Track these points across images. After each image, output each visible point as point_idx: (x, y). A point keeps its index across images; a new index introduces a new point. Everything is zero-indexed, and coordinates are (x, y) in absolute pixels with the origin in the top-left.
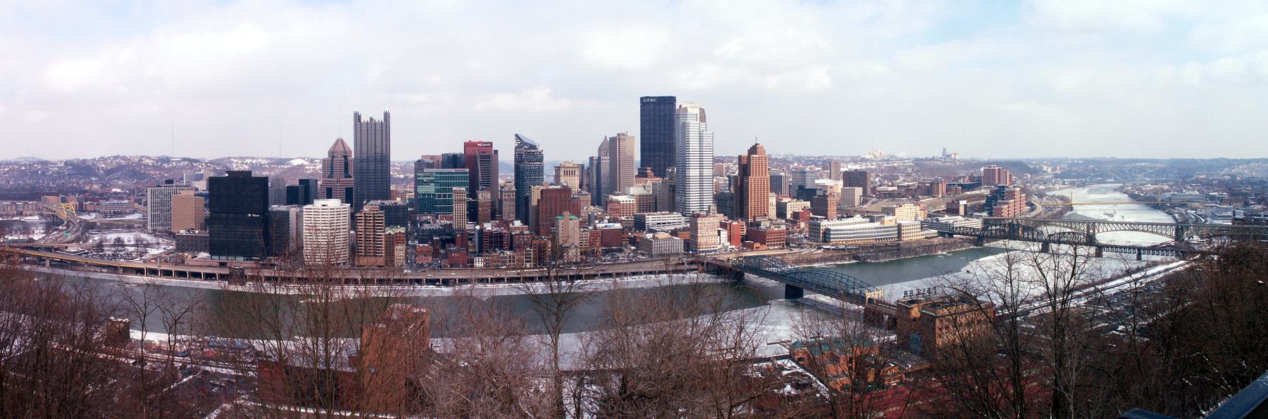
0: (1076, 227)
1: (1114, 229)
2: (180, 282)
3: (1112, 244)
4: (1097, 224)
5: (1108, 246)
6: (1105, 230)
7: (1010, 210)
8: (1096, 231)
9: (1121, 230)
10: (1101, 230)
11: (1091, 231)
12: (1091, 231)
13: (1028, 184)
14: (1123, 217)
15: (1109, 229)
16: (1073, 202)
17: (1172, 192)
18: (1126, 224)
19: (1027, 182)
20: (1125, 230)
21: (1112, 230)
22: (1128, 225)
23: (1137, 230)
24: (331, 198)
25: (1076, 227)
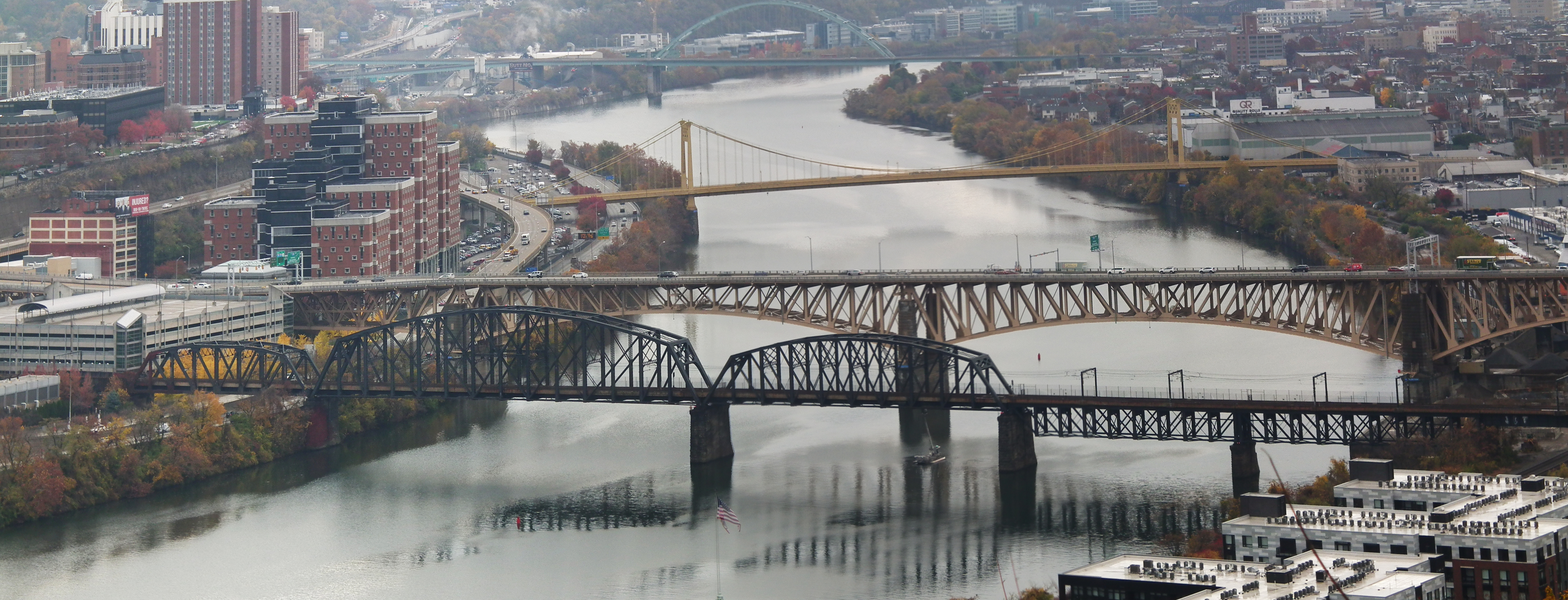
5: (1064, 404)
23: (1183, 313)
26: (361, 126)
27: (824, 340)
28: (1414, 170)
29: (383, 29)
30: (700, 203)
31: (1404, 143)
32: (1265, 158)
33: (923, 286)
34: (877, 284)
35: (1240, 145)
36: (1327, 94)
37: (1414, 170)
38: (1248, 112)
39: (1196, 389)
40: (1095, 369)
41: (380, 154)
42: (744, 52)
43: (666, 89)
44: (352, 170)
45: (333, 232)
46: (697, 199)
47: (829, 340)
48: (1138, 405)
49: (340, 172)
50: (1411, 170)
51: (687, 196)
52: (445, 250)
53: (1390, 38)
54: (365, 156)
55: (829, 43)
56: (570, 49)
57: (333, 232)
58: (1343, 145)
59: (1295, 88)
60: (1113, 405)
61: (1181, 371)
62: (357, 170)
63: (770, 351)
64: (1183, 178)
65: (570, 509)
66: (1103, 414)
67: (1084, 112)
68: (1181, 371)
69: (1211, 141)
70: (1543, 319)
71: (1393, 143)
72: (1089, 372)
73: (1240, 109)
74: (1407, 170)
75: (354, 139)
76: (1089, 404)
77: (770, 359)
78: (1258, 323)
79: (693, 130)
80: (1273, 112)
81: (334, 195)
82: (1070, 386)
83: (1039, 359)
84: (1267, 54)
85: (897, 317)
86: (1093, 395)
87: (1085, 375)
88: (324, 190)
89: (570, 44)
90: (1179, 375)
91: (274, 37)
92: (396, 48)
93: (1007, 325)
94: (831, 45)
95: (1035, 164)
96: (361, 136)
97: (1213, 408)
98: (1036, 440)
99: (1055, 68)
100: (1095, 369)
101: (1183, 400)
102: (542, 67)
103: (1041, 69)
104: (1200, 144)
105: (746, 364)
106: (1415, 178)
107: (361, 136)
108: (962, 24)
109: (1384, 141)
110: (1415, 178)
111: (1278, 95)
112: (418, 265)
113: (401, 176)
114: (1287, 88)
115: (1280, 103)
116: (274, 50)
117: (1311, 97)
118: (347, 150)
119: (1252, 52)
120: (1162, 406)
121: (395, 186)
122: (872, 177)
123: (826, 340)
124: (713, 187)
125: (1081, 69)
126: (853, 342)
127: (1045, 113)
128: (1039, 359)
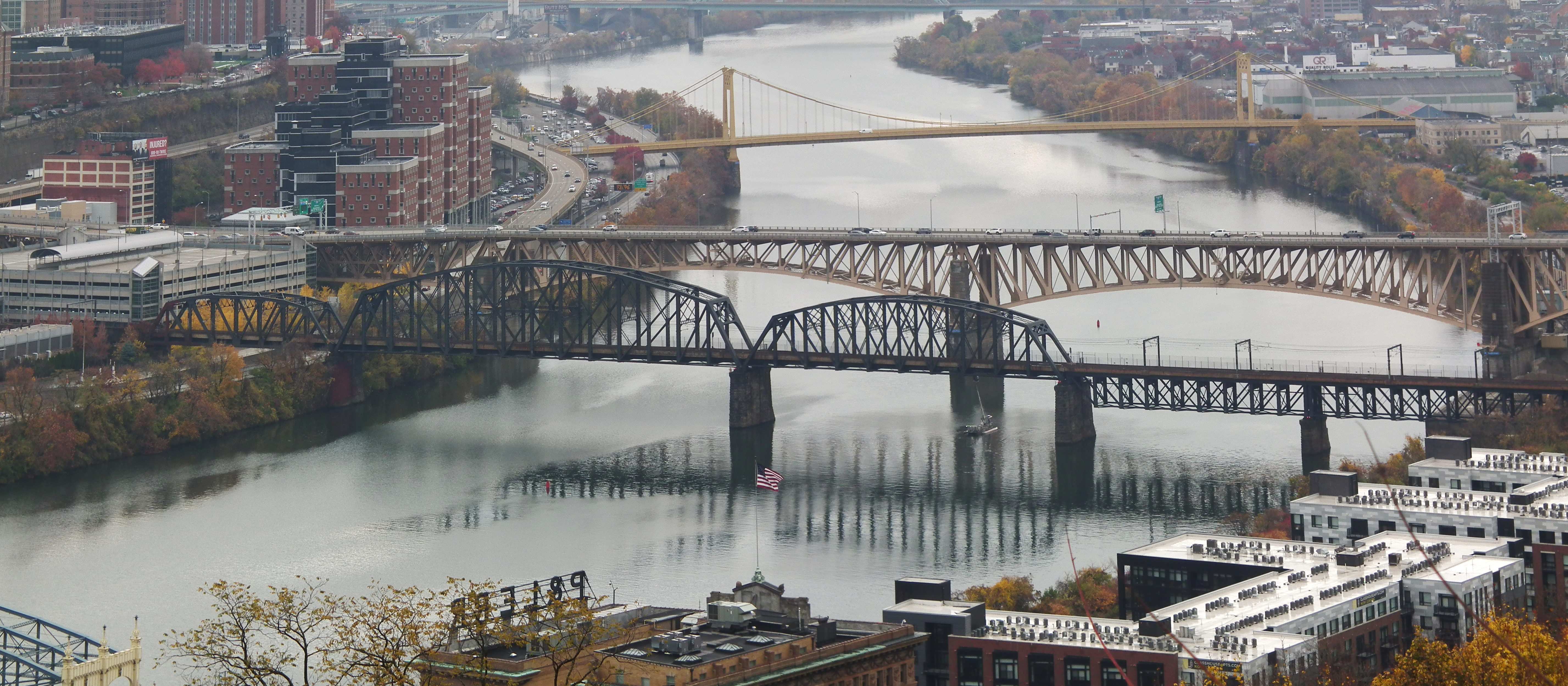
5: (1125, 374)
23: (1252, 279)
26: (389, 69)
27: (871, 301)
28: (1496, 133)
30: (742, 154)
31: (1485, 104)
32: (1339, 117)
35: (1314, 103)
36: (1405, 51)
37: (1496, 133)
38: (1322, 69)
41: (408, 98)
44: (379, 115)
48: (1203, 377)
49: (367, 116)
50: (1492, 132)
51: (729, 147)
52: (475, 200)
54: (393, 100)
60: (1177, 376)
61: (1249, 341)
63: (814, 312)
64: (1253, 137)
68: (1249, 341)
73: (1314, 65)
74: (1489, 133)
75: (381, 83)
77: (814, 320)
79: (736, 78)
80: (1348, 69)
82: (1132, 356)
83: (1098, 326)
84: (1342, 7)
86: (1156, 364)
87: (1147, 344)
88: (350, 136)
90: (1247, 345)
93: (1066, 289)
96: (389, 80)
97: (1282, 380)
99: (1119, 17)
101: (1251, 372)
102: (578, 10)
103: (1104, 18)
105: (789, 325)
107: (389, 80)
112: (447, 215)
115: (1356, 60)
118: (374, 94)
120: (1228, 378)
125: (1146, 20)
126: (902, 304)
127: (1107, 66)
128: (1098, 326)
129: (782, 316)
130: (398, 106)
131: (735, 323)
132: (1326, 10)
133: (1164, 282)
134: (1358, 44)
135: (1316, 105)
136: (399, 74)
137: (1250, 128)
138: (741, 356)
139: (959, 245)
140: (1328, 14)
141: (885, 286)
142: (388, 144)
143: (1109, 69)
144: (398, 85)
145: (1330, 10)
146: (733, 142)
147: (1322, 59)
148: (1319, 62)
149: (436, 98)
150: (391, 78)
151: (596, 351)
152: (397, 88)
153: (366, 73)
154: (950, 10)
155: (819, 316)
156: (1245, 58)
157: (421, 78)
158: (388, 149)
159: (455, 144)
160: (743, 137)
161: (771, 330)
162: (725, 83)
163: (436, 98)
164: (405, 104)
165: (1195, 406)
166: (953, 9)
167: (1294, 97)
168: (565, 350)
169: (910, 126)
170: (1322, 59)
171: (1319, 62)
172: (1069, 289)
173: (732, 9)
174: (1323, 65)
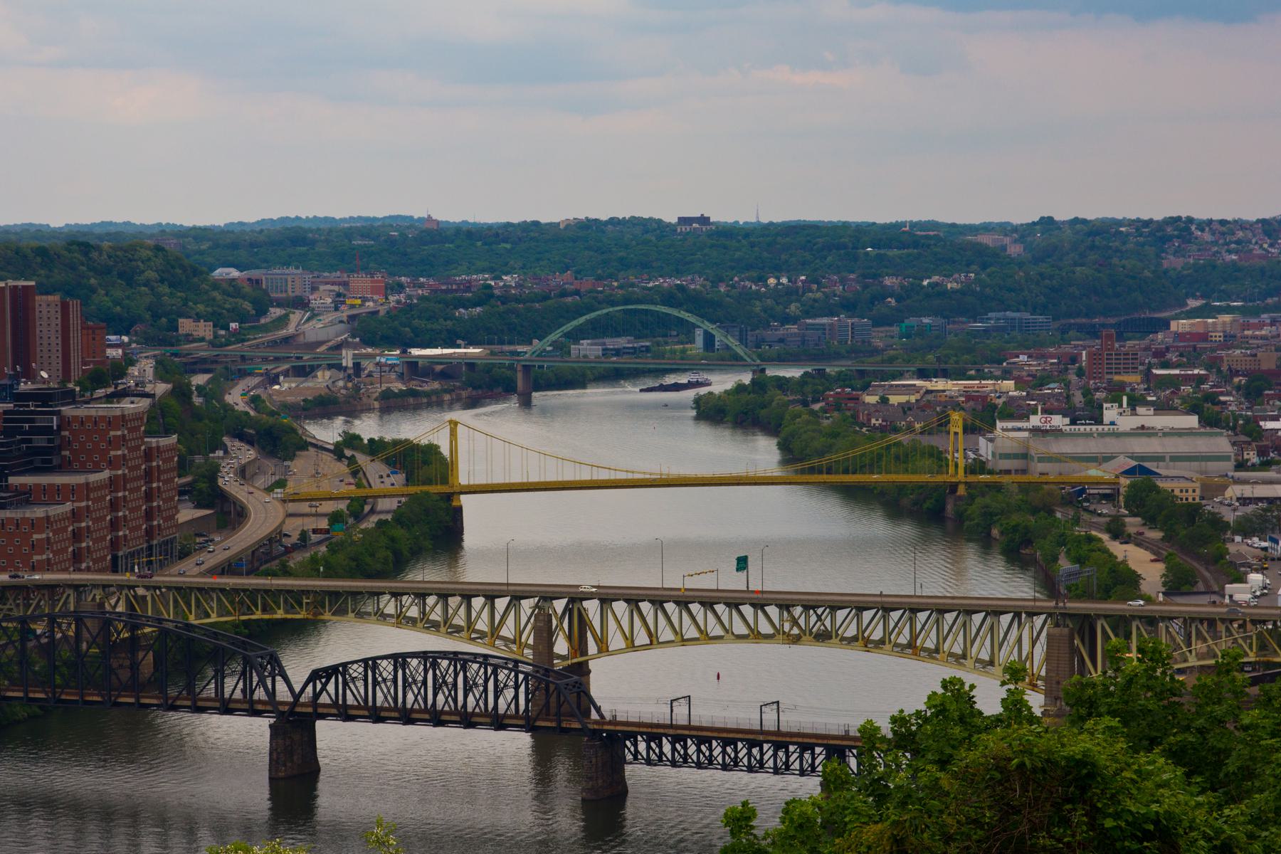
0: (495, 630)
1: (691, 632)
2: (1193, 325)
3: (681, 715)
4: (592, 607)
5: (653, 733)
6: (641, 638)
7: (861, 642)
8: (592, 648)
9: (729, 635)
10: (616, 642)
11: (561, 646)
12: (561, 646)
13: (200, 379)
14: (742, 563)
15: (666, 634)
16: (463, 479)
17: (1035, 420)
18: (759, 605)
19: (198, 366)
20: (755, 635)
21: (684, 641)
22: (773, 611)
23: (823, 637)
24: (831, 474)
25: (495, 630)
26: (55, 418)
27: (409, 657)
28: (1194, 491)
29: (282, 321)
30: (465, 500)
31: (1203, 463)
32: (1060, 474)
33: (565, 601)
34: (517, 597)
35: (1036, 460)
36: (1152, 412)
37: (1194, 491)
38: (1048, 428)
39: (793, 721)
40: (689, 696)
41: (76, 446)
42: (629, 353)
43: (539, 387)
44: (44, 461)
45: (33, 523)
46: (463, 497)
47: (417, 658)
48: (729, 737)
49: (31, 462)
50: (1190, 490)
51: (453, 494)
52: (155, 542)
53: (1248, 359)
54: (60, 448)
55: (716, 347)
56: (459, 347)
57: (33, 523)
58: (1134, 463)
59: (1121, 406)
60: (704, 736)
61: (778, 702)
62: (50, 461)
63: (384, 663)
64: (961, 490)
65: (542, 774)
66: (693, 742)
67: (911, 422)
68: (778, 702)
69: (1010, 454)
70: (1195, 659)
71: (1193, 463)
72: (680, 701)
73: (1039, 424)
74: (1187, 491)
75: (47, 430)
76: (679, 735)
77: (385, 674)
78: (902, 650)
79: (460, 429)
80: (1100, 428)
81: (16, 486)
82: (656, 712)
83: (718, 678)
84: (1130, 370)
85: (532, 633)
86: (686, 723)
87: (674, 704)
88: (7, 481)
89: (459, 342)
90: (775, 706)
91: (53, 325)
92: (287, 340)
93: (649, 642)
94: (718, 349)
95: (820, 472)
96: (55, 428)
97: (806, 743)
98: (628, 768)
99: (915, 376)
100: (689, 696)
101: (778, 733)
102: (417, 362)
103: (900, 375)
104: (998, 457)
105: (333, 680)
106: (1194, 499)
107: (55, 428)
108: (852, 333)
109: (1223, 461)
110: (1194, 499)
111: (1105, 411)
112: (115, 559)
113: (97, 469)
114: (1114, 405)
115: (1106, 419)
116: (53, 338)
117: (1136, 415)
118: (40, 441)
119: (1107, 368)
120: (754, 739)
121: (93, 478)
122: (642, 480)
123: (413, 657)
124: (531, 484)
125: (935, 380)
126: (439, 661)
127: (873, 421)
128: (718, 678)
129: (325, 670)
130: (67, 453)
131: (281, 675)
132: (1107, 373)
133: (741, 637)
134: (1109, 405)
135: (1039, 462)
136: (65, 422)
137: (960, 482)
138: (281, 708)
139: (546, 596)
140: (1109, 376)
141: (473, 636)
142: (73, 490)
143: (874, 424)
144: (66, 433)
145: (1111, 373)
146: (457, 489)
147: (1049, 419)
148: (1046, 422)
149: (103, 445)
150: (57, 426)
151: (200, 704)
152: (65, 436)
153: (32, 421)
154: (761, 367)
155: (391, 668)
156: (957, 418)
157: (89, 426)
158: (45, 495)
159: (125, 490)
160: (591, 480)
161: (311, 684)
162: (451, 435)
163: (103, 445)
164: (72, 451)
165: (745, 766)
166: (764, 367)
167: (1014, 454)
168: (170, 702)
169: (630, 476)
170: (1049, 419)
171: (1046, 422)
172: (651, 643)
173: (580, 365)
174: (1048, 425)
